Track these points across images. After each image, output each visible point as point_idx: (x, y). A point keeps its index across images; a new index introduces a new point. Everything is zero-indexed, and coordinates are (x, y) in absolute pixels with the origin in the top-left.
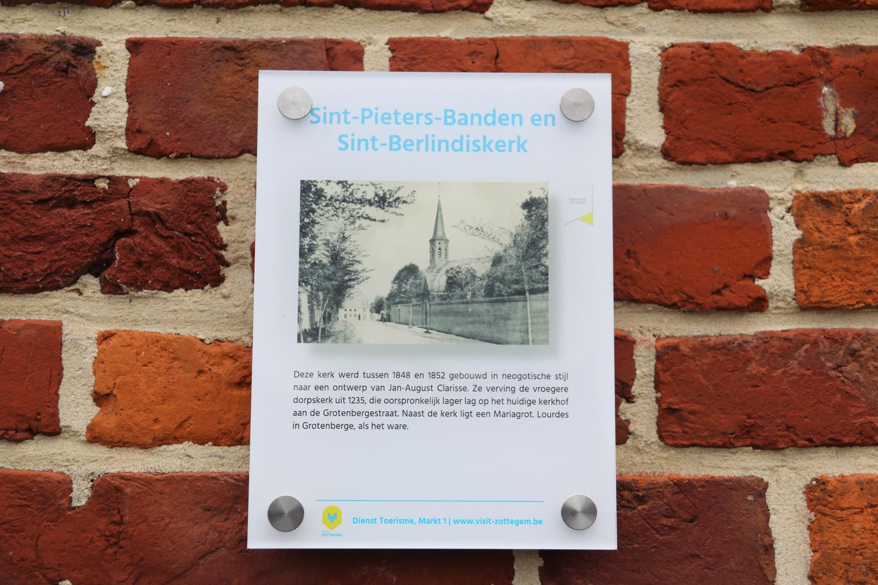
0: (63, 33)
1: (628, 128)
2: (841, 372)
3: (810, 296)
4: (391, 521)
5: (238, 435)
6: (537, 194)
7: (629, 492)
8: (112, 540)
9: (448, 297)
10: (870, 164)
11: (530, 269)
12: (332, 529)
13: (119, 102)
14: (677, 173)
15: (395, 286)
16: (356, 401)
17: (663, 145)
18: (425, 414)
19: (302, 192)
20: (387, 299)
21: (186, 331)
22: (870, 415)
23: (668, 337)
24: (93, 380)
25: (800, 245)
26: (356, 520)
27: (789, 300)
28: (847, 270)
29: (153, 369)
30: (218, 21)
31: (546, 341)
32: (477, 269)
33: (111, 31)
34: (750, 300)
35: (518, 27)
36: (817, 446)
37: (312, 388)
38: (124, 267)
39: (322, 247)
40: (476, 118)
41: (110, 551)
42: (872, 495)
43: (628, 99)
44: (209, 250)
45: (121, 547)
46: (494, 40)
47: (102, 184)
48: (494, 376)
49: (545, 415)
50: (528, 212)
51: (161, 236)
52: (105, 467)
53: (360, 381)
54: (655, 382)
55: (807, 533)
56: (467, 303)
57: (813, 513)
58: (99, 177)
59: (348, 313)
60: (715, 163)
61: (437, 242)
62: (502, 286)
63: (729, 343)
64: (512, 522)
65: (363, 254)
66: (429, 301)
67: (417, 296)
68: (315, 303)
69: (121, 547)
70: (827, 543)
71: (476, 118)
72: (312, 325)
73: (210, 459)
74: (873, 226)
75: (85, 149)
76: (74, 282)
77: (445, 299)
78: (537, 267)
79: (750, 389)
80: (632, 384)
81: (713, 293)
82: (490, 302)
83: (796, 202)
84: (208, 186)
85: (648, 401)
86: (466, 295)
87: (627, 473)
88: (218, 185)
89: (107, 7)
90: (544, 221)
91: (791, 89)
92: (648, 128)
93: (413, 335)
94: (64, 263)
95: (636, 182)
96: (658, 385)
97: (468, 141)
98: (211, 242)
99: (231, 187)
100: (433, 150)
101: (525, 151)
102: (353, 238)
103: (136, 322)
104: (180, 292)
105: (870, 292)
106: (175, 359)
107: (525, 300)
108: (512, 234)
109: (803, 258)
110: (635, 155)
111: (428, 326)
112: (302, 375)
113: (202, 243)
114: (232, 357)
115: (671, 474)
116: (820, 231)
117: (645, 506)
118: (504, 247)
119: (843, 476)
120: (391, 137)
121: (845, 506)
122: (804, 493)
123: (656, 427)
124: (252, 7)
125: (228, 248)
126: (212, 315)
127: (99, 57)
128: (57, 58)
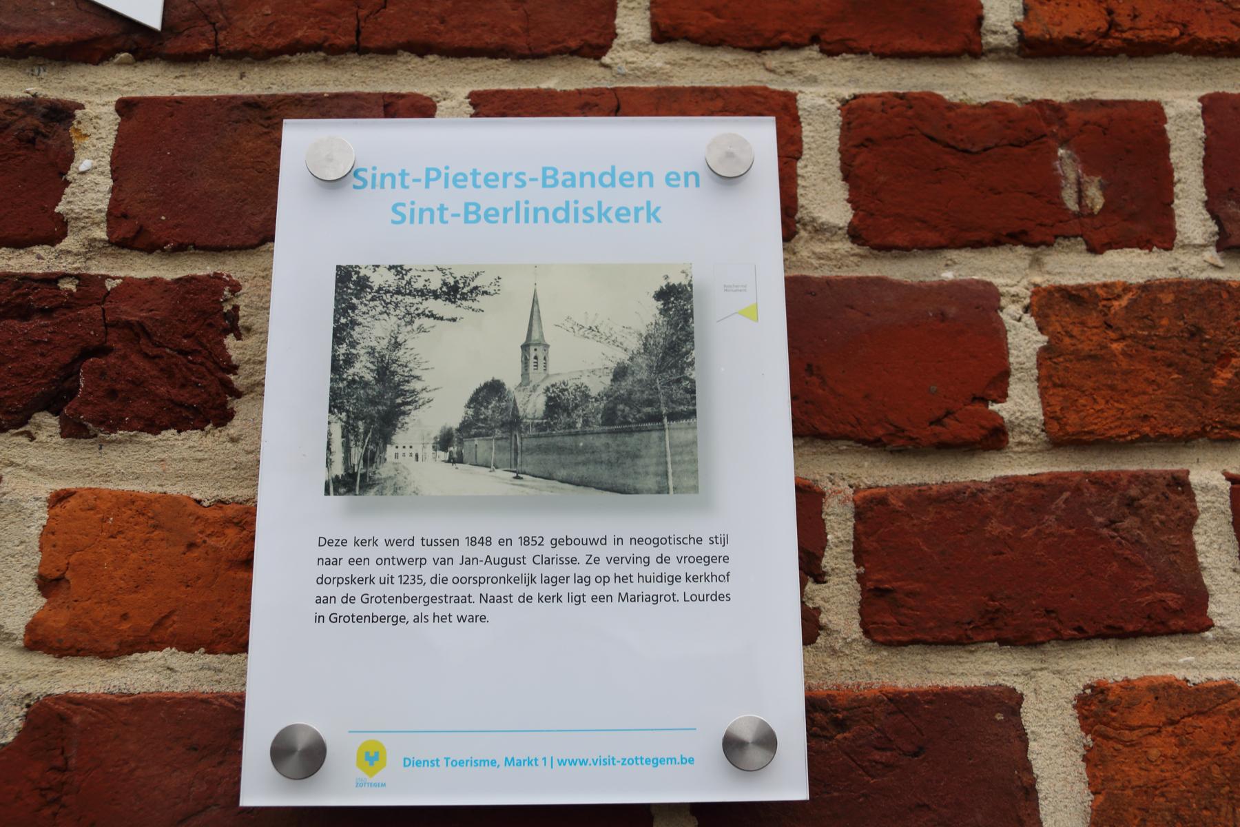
0: (35, 96)
1: (801, 201)
2: (1115, 530)
3: (1066, 424)
4: (461, 763)
5: (235, 640)
6: (676, 280)
7: (823, 713)
8: (51, 795)
9: (548, 425)
10: (1128, 250)
11: (668, 384)
12: (371, 775)
13: (100, 179)
14: (872, 262)
15: (471, 412)
16: (410, 581)
17: (850, 224)
18: (515, 599)
19: (337, 281)
20: (458, 430)
21: (175, 489)
22: (1160, 590)
23: (870, 488)
24: (38, 559)
25: (1045, 356)
26: (408, 762)
27: (1037, 431)
28: (1112, 388)
29: (125, 542)
30: (242, 76)
31: (695, 489)
32: (590, 386)
33: (99, 92)
34: (984, 432)
35: (646, 76)
36: (1089, 638)
37: (345, 562)
38: (91, 398)
39: (364, 358)
40: (587, 179)
41: (47, 812)
42: (1172, 707)
43: (800, 164)
44: (212, 374)
45: (63, 806)
46: (615, 90)
47: (68, 286)
48: (618, 541)
49: (696, 598)
50: (664, 305)
51: (146, 356)
52: (48, 686)
53: (418, 551)
54: (855, 551)
55: (1082, 766)
56: (577, 434)
57: (1089, 737)
58: (65, 276)
59: (400, 451)
60: (922, 248)
61: (532, 348)
62: (627, 409)
63: (958, 492)
64: (648, 761)
65: (424, 366)
66: (520, 432)
67: (503, 425)
68: (352, 438)
69: (63, 806)
70: (1113, 780)
71: (587, 179)
72: (346, 470)
73: (201, 674)
74: (1142, 329)
75: (53, 245)
76: (25, 423)
77: (545, 430)
78: (678, 381)
79: (991, 558)
80: (823, 556)
81: (931, 423)
82: (610, 432)
83: (1036, 299)
84: (215, 283)
85: (846, 579)
86: (575, 423)
87: (819, 686)
88: (227, 283)
89: (96, 64)
90: (687, 316)
91: (1017, 150)
92: (829, 202)
93: (497, 482)
94: (7, 393)
95: (817, 274)
96: (860, 555)
97: (576, 210)
98: (215, 363)
99: (246, 287)
100: (527, 221)
101: (658, 221)
102: (410, 344)
103: (106, 477)
104: (170, 434)
105: (1146, 418)
106: (156, 527)
107: (662, 429)
108: (641, 335)
109: (1053, 372)
110: (812, 238)
111: (519, 468)
112: (329, 543)
113: (202, 364)
114: (237, 524)
115: (883, 686)
116: (1072, 336)
117: (846, 735)
118: (630, 354)
119: (1129, 681)
120: (467, 205)
121: (1135, 723)
122: (1075, 707)
123: (858, 616)
124: (287, 57)
125: (239, 371)
126: (214, 465)
127: (79, 123)
128: (21, 125)
